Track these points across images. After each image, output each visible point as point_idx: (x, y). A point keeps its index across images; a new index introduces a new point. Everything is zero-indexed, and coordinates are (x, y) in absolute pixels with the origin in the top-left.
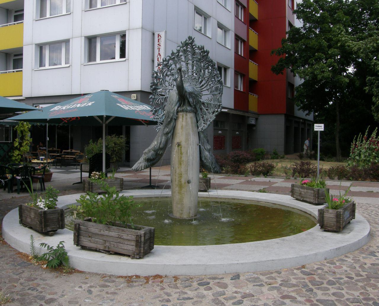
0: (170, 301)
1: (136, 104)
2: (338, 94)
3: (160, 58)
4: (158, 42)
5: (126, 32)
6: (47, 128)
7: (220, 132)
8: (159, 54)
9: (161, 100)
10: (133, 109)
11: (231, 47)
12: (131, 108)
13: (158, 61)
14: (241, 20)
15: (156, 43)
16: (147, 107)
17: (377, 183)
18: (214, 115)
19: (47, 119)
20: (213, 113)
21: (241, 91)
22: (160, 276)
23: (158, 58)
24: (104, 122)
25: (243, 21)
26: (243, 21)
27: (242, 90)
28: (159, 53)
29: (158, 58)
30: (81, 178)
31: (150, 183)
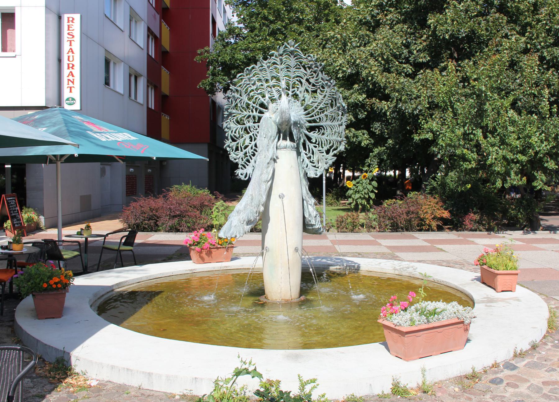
0: (543, 382)
1: (112, 131)
2: (408, 128)
3: (73, 56)
4: (69, 30)
5: (15, 10)
6: (324, 182)
7: (150, 170)
8: (71, 51)
9: (239, 131)
10: (113, 139)
11: (144, 47)
12: (108, 137)
13: (69, 60)
14: (152, 5)
15: (65, 31)
16: (130, 136)
17: (427, 233)
18: (331, 153)
19: (74, 155)
20: (328, 152)
21: (152, 109)
22: (131, 371)
23: (69, 57)
24: (59, 159)
25: (154, 7)
26: (154, 7)
27: (153, 108)
28: (71, 49)
29: (69, 57)
30: (104, 241)
31: (104, 244)
